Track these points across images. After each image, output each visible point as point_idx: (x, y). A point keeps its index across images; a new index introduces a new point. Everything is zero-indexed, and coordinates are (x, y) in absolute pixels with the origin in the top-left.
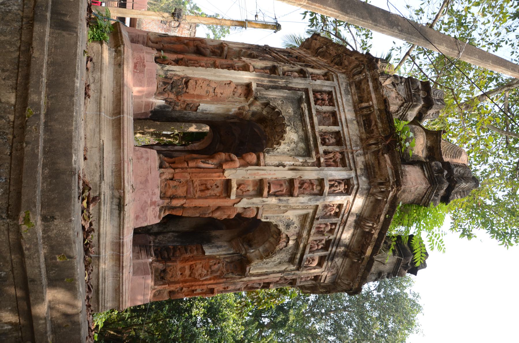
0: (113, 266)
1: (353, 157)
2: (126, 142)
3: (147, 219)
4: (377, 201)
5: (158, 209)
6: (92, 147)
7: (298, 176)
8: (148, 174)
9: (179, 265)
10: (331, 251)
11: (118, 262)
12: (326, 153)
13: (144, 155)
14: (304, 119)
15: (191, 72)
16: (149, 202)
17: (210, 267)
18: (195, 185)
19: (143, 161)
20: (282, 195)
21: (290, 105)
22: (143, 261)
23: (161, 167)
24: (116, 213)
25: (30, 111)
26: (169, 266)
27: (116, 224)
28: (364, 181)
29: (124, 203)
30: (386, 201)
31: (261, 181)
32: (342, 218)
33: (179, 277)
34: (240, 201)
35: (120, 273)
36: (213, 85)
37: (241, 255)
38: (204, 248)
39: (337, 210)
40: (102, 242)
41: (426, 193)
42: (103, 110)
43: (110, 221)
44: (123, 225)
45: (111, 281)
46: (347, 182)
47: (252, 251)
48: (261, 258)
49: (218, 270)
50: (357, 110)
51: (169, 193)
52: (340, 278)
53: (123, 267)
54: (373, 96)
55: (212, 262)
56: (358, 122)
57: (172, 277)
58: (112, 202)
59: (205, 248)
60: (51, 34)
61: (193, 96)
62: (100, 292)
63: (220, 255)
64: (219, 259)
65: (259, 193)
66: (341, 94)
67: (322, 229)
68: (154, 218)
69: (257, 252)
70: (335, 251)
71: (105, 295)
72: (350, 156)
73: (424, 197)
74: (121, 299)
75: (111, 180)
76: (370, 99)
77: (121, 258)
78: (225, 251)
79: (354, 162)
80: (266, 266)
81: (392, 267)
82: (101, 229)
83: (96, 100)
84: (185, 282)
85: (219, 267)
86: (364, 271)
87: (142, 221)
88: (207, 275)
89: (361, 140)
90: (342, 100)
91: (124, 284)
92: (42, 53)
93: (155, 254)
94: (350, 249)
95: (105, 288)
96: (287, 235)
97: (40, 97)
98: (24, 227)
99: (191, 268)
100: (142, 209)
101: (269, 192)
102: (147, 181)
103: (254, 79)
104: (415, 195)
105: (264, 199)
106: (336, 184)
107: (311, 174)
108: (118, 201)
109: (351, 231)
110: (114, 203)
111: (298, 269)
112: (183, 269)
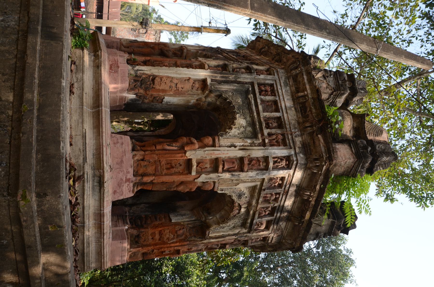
0: (95, 233)
2: (104, 130)
3: (123, 193)
4: (313, 174)
5: (132, 185)
6: (76, 135)
8: (123, 156)
9: (150, 231)
10: (276, 216)
12: (270, 135)
13: (119, 141)
14: (251, 108)
15: (156, 71)
16: (124, 179)
19: (118, 145)
20: (234, 171)
22: (121, 228)
23: (133, 150)
24: (97, 189)
25: (25, 107)
26: (142, 232)
27: (97, 198)
29: (104, 180)
30: (321, 173)
31: (217, 160)
32: (285, 189)
33: (151, 241)
34: (199, 177)
35: (101, 239)
36: (175, 81)
37: (202, 222)
38: (171, 216)
41: (353, 166)
43: (93, 195)
46: (288, 158)
48: (219, 224)
49: (183, 234)
50: (295, 99)
51: (141, 172)
53: (104, 233)
54: (308, 87)
55: (177, 228)
56: (295, 109)
57: (145, 241)
58: (93, 180)
59: (171, 216)
60: (42, 43)
61: (159, 91)
62: (86, 255)
63: (184, 222)
65: (215, 170)
67: (269, 198)
68: (129, 193)
69: (215, 218)
71: (89, 258)
72: (290, 137)
73: (352, 169)
74: (103, 261)
75: (92, 162)
76: (305, 89)
79: (293, 142)
80: (223, 230)
82: (85, 203)
83: (79, 96)
84: (156, 245)
86: (304, 232)
87: (119, 195)
89: (299, 123)
95: (89, 251)
96: (239, 204)
98: (22, 203)
99: (160, 233)
100: (118, 185)
101: (223, 168)
102: (122, 161)
103: (209, 75)
105: (220, 175)
107: (258, 153)
108: (98, 179)
109: (293, 199)
111: (249, 232)
112: (153, 234)
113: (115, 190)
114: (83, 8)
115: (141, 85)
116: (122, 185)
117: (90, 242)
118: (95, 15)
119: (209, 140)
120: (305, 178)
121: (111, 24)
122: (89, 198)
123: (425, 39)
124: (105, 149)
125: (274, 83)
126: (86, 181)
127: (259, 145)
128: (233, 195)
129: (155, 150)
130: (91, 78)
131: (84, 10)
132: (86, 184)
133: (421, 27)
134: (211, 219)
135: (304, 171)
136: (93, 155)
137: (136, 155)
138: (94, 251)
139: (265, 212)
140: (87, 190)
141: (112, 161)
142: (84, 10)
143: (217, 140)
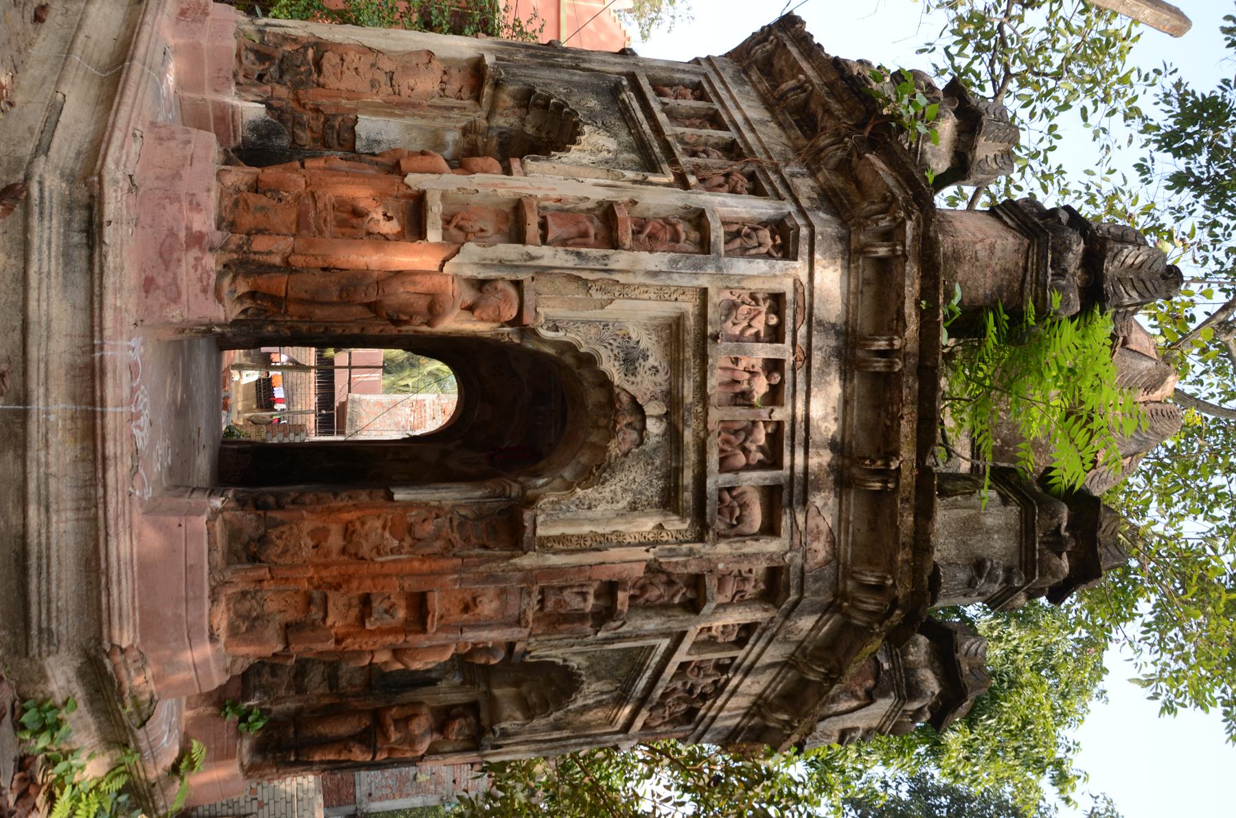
0: (75, 461)
1: (783, 181)
3: (179, 294)
4: (883, 265)
7: (626, 199)
8: (183, 165)
10: (792, 467)
11: (88, 443)
14: (631, 117)
16: (182, 235)
18: (320, 205)
24: (80, 255)
26: (277, 524)
27: (80, 297)
29: (101, 215)
30: (904, 251)
32: (794, 344)
34: (458, 252)
35: (96, 486)
36: (388, 66)
39: (774, 321)
40: (33, 352)
41: (1025, 269)
43: (65, 286)
44: (101, 295)
45: (70, 526)
46: (779, 226)
47: (541, 482)
49: (437, 537)
50: (771, 103)
51: (247, 221)
52: (849, 574)
53: (104, 458)
57: (285, 552)
58: (68, 223)
62: (33, 561)
67: (745, 386)
68: (201, 296)
70: (806, 467)
71: (49, 582)
72: (773, 177)
73: (1023, 281)
74: (104, 600)
75: (70, 164)
77: (99, 421)
80: (590, 514)
81: (1013, 544)
82: (33, 304)
85: (439, 529)
86: (915, 521)
87: (162, 299)
89: (797, 150)
90: (729, 91)
91: (112, 531)
94: (850, 456)
95: (48, 548)
96: (633, 399)
99: (348, 532)
100: (161, 255)
104: (995, 274)
105: (531, 249)
108: (85, 213)
109: (835, 389)
110: (75, 226)
112: (319, 536)
113: (149, 273)
114: (280, 401)
115: (281, 77)
116: (175, 256)
117: (52, 499)
118: (313, 417)
120: (859, 293)
122: (49, 288)
123: (1207, 240)
126: (36, 210)
128: (604, 353)
131: (283, 406)
132: (35, 221)
133: (1185, 213)
134: (543, 486)
135: (847, 268)
136: (79, 154)
138: (70, 555)
139: (746, 451)
140: (40, 253)
142: (283, 406)
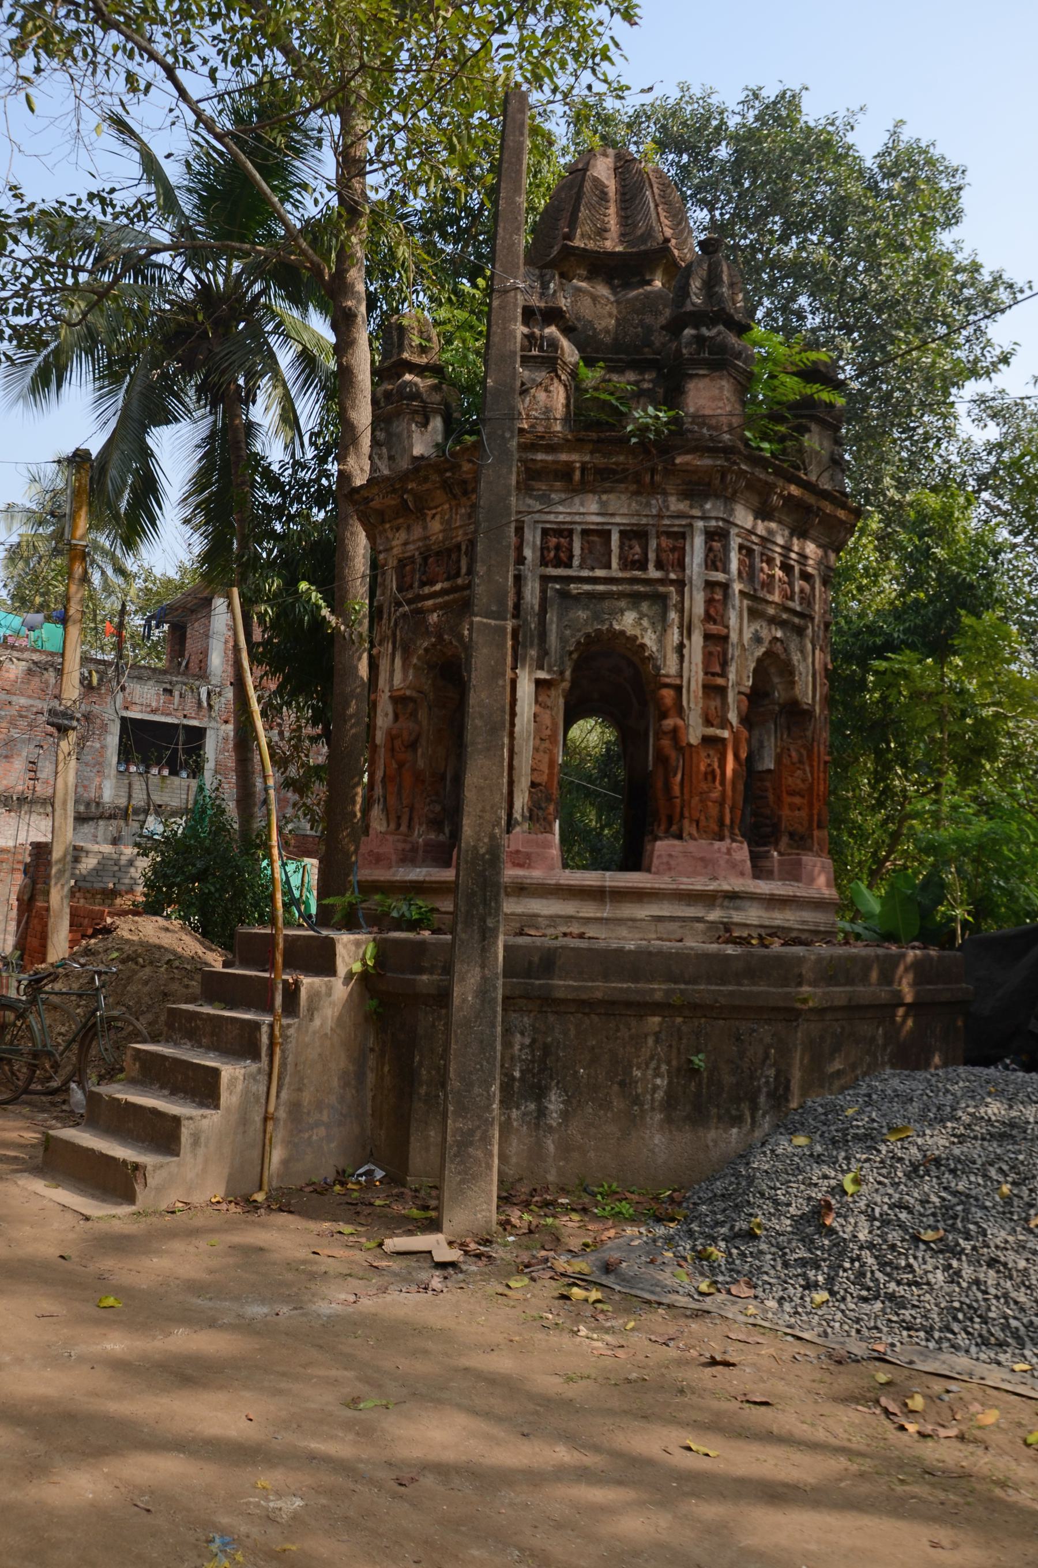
2: (649, 885)
5: (734, 845)
6: (656, 932)
9: (786, 812)
12: (659, 565)
13: (665, 860)
15: (523, 779)
17: (793, 764)
19: (673, 863)
20: (725, 653)
21: (571, 615)
22: (776, 864)
23: (679, 837)
24: (738, 902)
25: (676, 1000)
28: (713, 505)
31: (705, 687)
33: (803, 814)
37: (781, 712)
38: (760, 768)
41: (739, 383)
42: (599, 915)
46: (711, 535)
48: (793, 683)
49: (798, 751)
50: (584, 488)
54: (564, 457)
55: (786, 760)
56: (605, 492)
57: (801, 824)
59: (760, 768)
60: (560, 978)
61: (551, 775)
63: (776, 746)
64: (782, 749)
65: (722, 691)
66: (550, 513)
69: (779, 687)
72: (666, 522)
76: (569, 464)
78: (769, 740)
79: (678, 517)
83: (585, 924)
84: (811, 805)
88: (804, 771)
89: (637, 493)
92: (597, 988)
93: (765, 845)
97: (658, 990)
98: (811, 1004)
99: (792, 793)
101: (718, 675)
102: (702, 859)
103: (530, 673)
106: (711, 555)
107: (697, 602)
111: (812, 619)
112: (793, 807)
119: (668, 695)
121: (66, 818)
124: (682, 887)
125: (541, 525)
127: (681, 594)
129: (683, 800)
130: (544, 901)
137: (690, 834)
141: (701, 874)
143: (668, 680)
